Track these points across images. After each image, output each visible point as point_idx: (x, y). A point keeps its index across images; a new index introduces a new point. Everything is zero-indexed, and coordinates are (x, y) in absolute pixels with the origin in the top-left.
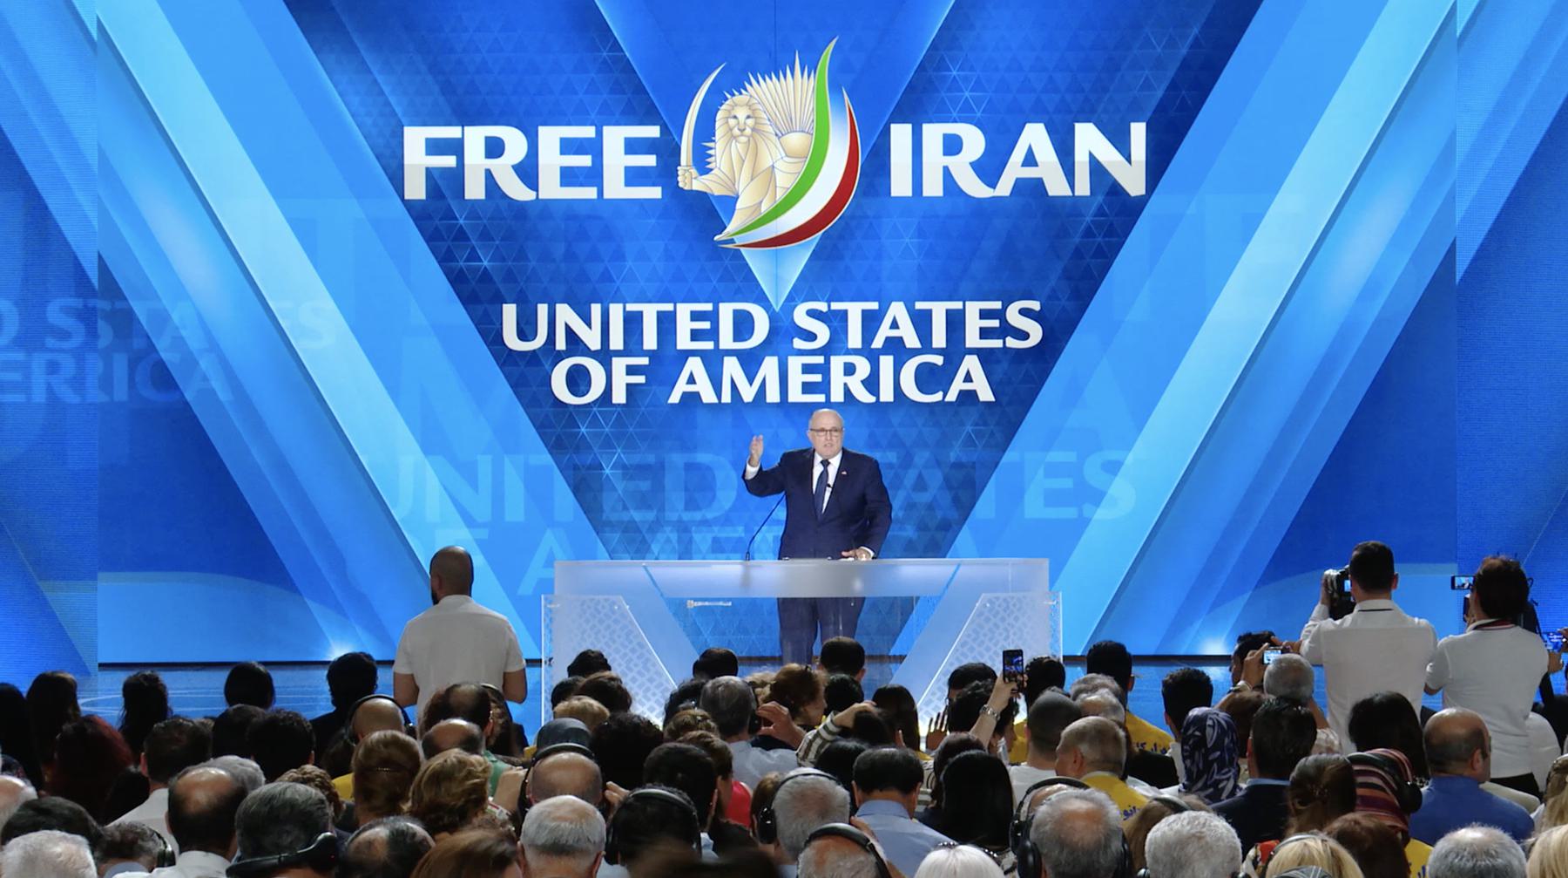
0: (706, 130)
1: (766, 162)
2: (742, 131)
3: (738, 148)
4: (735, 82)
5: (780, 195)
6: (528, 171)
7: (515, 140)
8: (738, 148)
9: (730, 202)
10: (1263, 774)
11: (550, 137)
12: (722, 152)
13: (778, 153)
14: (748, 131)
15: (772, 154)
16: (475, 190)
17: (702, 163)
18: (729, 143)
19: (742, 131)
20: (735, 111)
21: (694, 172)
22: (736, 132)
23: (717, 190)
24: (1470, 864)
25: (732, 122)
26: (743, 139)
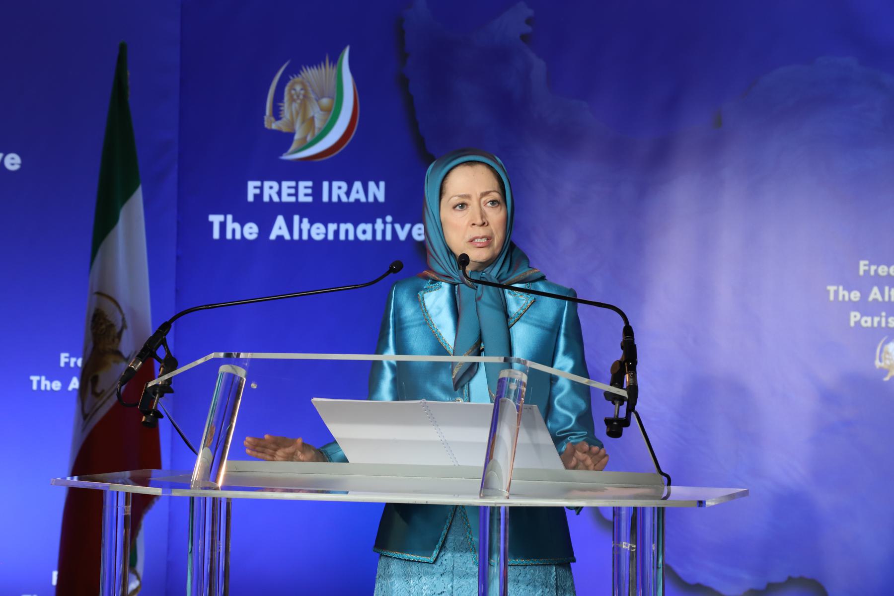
0: (279, 97)
1: (311, 114)
2: (298, 96)
3: (295, 106)
4: (294, 71)
5: (317, 132)
6: (279, 193)
7: (275, 185)
8: (295, 106)
9: (290, 137)
10: (386, 346)
11: (285, 184)
12: (288, 109)
13: (317, 109)
14: (301, 97)
15: (316, 113)
16: (266, 199)
17: (277, 115)
18: (290, 105)
19: (298, 96)
20: (295, 87)
21: (273, 119)
22: (295, 97)
23: (285, 129)
24: (423, 580)
25: (293, 92)
26: (299, 101)
